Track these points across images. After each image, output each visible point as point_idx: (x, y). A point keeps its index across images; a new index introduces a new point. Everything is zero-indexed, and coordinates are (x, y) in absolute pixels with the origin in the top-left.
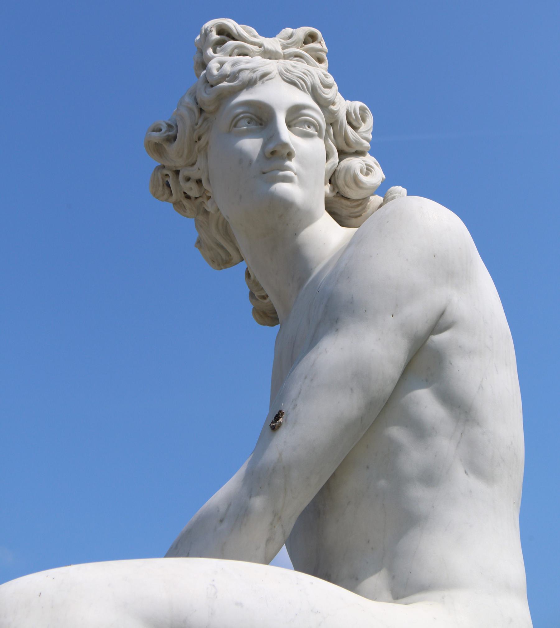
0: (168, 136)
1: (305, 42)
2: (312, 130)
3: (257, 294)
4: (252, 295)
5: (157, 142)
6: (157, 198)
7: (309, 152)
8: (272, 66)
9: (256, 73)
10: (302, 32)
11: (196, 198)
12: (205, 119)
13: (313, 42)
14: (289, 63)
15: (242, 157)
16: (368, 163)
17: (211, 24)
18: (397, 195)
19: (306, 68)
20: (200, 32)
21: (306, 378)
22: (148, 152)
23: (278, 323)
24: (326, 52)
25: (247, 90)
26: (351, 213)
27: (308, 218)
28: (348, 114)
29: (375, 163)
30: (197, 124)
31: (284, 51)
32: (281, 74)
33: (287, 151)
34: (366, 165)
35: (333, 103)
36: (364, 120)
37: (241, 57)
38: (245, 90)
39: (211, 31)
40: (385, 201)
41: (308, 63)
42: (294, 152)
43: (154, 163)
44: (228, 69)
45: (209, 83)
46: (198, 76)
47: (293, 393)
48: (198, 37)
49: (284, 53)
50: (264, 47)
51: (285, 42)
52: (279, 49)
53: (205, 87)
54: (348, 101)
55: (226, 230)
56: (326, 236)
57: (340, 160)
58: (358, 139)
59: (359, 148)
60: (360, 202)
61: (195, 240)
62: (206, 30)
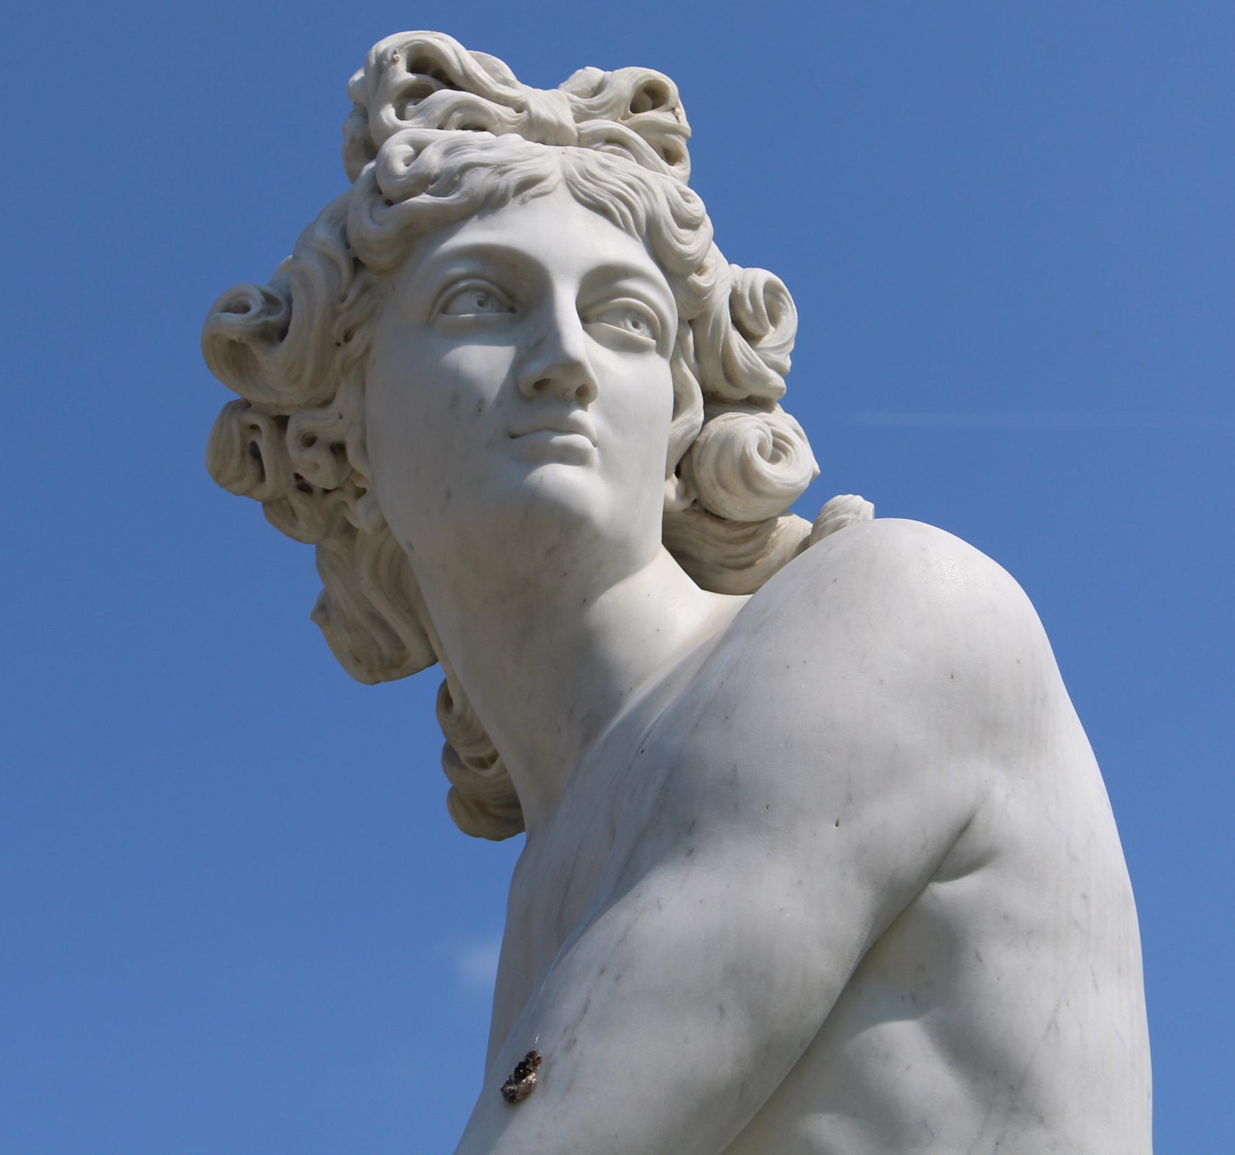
0: (266, 324)
1: (636, 108)
2: (641, 334)
3: (463, 754)
4: (450, 755)
5: (235, 338)
6: (223, 486)
7: (631, 387)
8: (549, 161)
9: (505, 176)
10: (627, 79)
11: (326, 491)
12: (366, 288)
13: (654, 107)
14: (593, 157)
15: (460, 389)
16: (778, 430)
17: (388, 44)
18: (850, 516)
19: (632, 171)
20: (364, 63)
21: (602, 971)
22: (209, 364)
23: (520, 828)
24: (685, 136)
25: (480, 218)
26: (727, 557)
27: (618, 560)
28: (735, 300)
29: (796, 431)
30: (343, 299)
31: (581, 125)
32: (570, 184)
33: (578, 383)
34: (775, 434)
35: (700, 269)
36: (774, 320)
37: (469, 134)
38: (475, 218)
39: (394, 61)
40: (819, 532)
41: (640, 159)
42: (595, 387)
43: (221, 392)
44: (433, 159)
45: (384, 194)
46: (353, 176)
47: (569, 1007)
48: (359, 76)
49: (579, 129)
50: (529, 112)
51: (583, 102)
52: (568, 119)
53: (372, 206)
54: (735, 266)
55: (397, 579)
56: (664, 610)
57: (708, 417)
58: (758, 366)
59: (756, 390)
60: (752, 529)
61: (312, 603)
62: (381, 58)
